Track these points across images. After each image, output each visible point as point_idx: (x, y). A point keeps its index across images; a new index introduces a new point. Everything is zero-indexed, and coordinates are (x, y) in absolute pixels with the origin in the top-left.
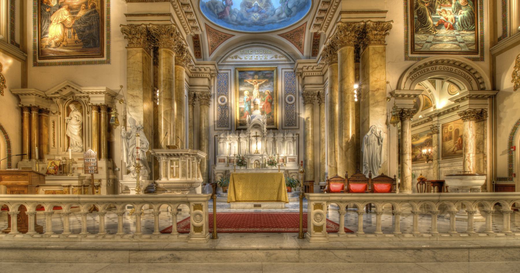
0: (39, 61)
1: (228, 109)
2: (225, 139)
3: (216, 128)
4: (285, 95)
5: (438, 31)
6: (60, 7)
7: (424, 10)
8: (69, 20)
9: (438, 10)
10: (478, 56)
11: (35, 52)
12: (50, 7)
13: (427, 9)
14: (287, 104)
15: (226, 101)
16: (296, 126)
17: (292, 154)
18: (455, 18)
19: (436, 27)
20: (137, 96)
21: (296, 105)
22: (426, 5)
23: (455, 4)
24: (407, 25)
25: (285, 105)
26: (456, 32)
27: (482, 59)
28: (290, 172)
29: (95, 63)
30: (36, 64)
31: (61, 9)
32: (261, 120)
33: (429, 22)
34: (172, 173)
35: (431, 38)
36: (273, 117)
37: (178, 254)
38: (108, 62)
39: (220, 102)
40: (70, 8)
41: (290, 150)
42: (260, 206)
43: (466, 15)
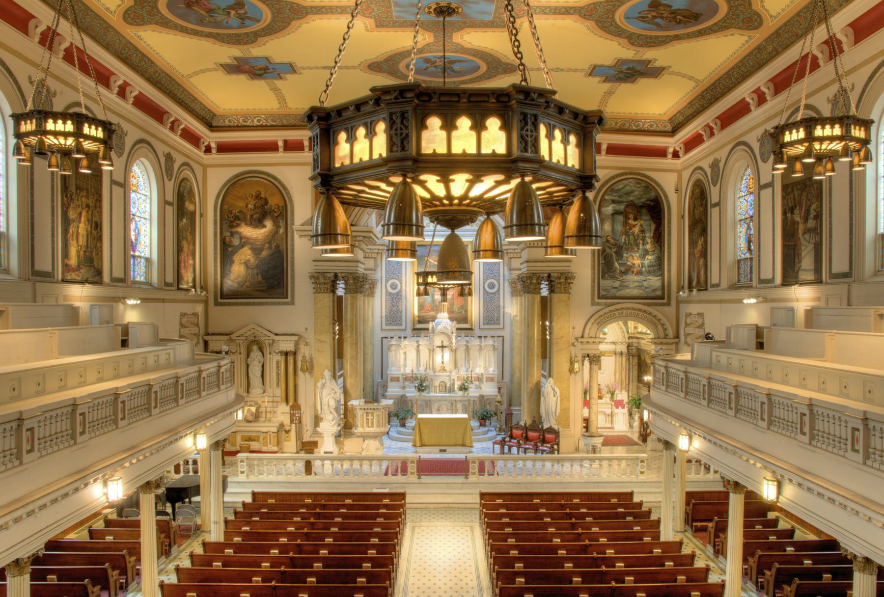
0: (220, 300)
1: (401, 299)
2: (399, 346)
3: (384, 327)
4: (484, 280)
5: (625, 277)
6: (243, 246)
7: (611, 256)
8: (252, 260)
9: (625, 255)
10: (665, 301)
11: (216, 292)
12: (233, 246)
13: (614, 254)
14: (487, 292)
15: (399, 288)
16: (499, 324)
17: (492, 370)
18: (642, 263)
19: (623, 273)
20: (324, 342)
21: (499, 294)
22: (614, 250)
23: (642, 249)
24: (594, 270)
25: (484, 294)
26: (641, 278)
27: (669, 304)
28: (485, 398)
29: (279, 304)
30: (217, 304)
31: (244, 249)
32: (449, 328)
33: (616, 268)
34: (368, 423)
35: (617, 284)
36: (466, 311)
37: (404, 485)
38: (292, 303)
39: (390, 290)
40: (252, 249)
41: (490, 362)
42: (445, 451)
43: (653, 260)
